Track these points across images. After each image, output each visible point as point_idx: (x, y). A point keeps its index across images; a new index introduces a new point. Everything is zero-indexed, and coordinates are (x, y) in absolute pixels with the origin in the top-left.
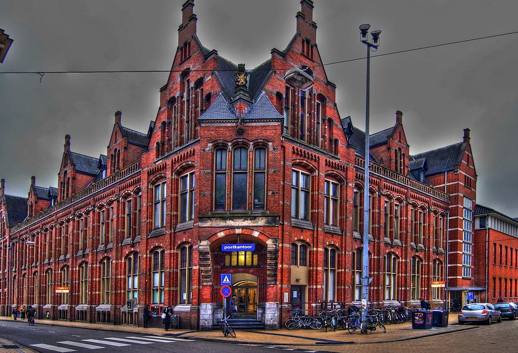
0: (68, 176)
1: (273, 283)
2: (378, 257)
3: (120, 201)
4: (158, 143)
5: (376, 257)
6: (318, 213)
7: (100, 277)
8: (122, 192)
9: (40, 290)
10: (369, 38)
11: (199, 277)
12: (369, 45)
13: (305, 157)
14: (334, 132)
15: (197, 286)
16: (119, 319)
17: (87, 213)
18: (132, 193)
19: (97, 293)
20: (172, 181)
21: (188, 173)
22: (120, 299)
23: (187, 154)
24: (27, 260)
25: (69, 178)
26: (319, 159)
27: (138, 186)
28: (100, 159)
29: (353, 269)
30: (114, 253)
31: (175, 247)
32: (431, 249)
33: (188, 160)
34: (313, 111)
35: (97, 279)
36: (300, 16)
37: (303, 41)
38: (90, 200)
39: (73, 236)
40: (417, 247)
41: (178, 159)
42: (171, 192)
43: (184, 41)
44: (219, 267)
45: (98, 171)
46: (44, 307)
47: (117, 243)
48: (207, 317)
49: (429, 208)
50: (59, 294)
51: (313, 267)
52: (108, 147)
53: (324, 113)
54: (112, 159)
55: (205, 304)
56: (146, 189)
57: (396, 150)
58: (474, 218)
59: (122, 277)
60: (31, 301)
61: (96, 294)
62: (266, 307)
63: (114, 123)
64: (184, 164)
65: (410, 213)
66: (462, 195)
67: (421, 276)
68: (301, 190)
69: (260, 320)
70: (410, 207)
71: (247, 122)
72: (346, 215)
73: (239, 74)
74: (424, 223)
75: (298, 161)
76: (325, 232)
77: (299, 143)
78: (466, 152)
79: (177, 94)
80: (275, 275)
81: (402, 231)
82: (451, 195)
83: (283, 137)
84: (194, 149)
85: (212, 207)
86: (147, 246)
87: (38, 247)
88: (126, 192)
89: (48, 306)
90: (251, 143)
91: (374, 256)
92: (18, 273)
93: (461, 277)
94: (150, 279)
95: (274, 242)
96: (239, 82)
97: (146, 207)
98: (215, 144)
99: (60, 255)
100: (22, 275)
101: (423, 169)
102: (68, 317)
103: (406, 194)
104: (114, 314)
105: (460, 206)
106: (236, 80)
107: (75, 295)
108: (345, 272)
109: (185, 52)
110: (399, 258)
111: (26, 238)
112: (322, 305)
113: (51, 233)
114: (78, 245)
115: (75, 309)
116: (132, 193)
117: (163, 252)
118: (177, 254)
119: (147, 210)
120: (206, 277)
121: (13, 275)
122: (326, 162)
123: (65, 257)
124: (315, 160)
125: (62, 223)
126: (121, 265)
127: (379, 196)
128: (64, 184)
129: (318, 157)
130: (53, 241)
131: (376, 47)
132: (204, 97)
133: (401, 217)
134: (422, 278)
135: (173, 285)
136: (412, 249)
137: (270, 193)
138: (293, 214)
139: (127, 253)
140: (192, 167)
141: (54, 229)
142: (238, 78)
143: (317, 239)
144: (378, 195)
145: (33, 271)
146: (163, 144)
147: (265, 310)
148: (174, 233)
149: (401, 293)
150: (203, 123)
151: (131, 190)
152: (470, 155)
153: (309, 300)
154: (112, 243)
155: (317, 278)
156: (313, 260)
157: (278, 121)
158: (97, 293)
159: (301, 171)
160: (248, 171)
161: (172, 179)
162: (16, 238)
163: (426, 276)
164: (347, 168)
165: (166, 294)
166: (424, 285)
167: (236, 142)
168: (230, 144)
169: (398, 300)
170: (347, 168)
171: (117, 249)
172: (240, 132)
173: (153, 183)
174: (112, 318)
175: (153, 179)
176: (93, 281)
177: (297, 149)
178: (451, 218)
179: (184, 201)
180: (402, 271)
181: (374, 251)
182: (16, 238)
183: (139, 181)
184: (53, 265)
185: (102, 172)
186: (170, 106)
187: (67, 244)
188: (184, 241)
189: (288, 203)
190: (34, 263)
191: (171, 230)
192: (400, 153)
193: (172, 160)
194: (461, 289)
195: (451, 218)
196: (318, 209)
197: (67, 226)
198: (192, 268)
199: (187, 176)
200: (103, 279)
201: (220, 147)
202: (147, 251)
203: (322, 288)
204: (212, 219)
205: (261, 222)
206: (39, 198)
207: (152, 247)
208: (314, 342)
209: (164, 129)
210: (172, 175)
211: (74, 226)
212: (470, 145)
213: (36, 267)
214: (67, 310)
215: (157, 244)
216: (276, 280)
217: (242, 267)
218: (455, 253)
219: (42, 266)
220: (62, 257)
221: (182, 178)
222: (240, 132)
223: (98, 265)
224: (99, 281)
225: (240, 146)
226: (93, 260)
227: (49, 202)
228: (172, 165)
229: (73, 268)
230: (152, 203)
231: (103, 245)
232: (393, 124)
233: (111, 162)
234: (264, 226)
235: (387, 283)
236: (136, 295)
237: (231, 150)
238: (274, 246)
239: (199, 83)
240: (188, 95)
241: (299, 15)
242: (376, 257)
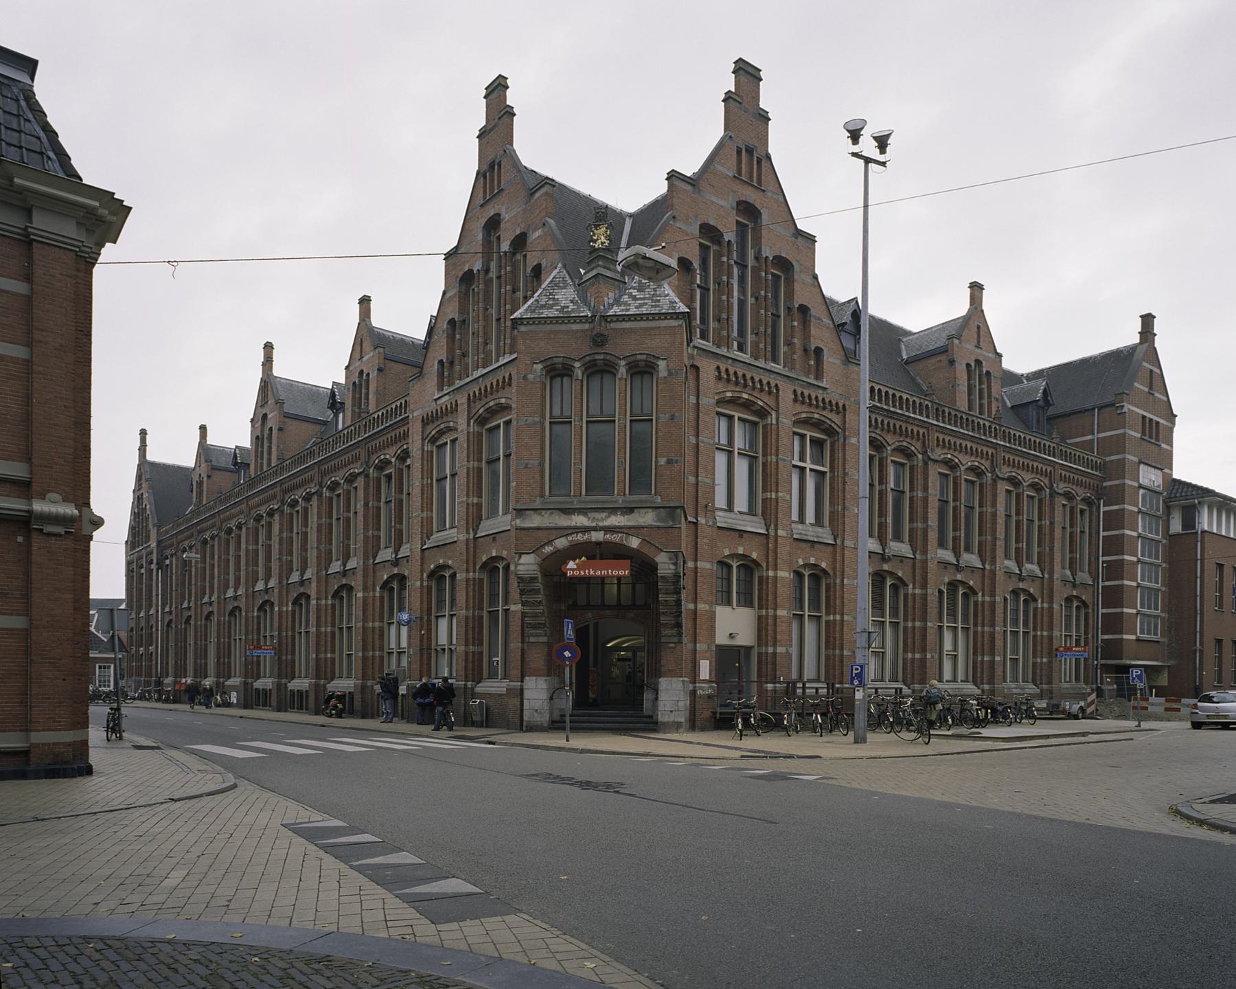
0: (269, 425)
1: (675, 639)
2: (924, 592)
3: (371, 476)
4: (441, 362)
5: (918, 591)
6: (777, 499)
7: (333, 625)
8: (478, 405)
9: (218, 649)
10: (868, 146)
11: (522, 627)
12: (868, 160)
13: (745, 386)
14: (812, 332)
15: (520, 644)
16: (372, 708)
17: (308, 498)
18: (393, 460)
19: (329, 655)
20: (468, 436)
21: (501, 421)
22: (373, 668)
23: (498, 385)
24: (193, 591)
25: (271, 429)
26: (778, 390)
27: (405, 447)
28: (332, 390)
29: (941, 620)
30: (360, 577)
31: (477, 568)
32: (1056, 576)
33: (500, 395)
34: (763, 293)
35: (329, 629)
36: (731, 100)
37: (739, 152)
38: (312, 472)
39: (280, 544)
40: (1020, 570)
41: (480, 393)
42: (468, 457)
43: (490, 158)
44: (563, 608)
45: (330, 415)
46: (226, 683)
47: (366, 558)
48: (537, 705)
49: (1051, 487)
50: (255, 659)
51: (767, 609)
52: (347, 368)
53: (790, 295)
54: (354, 391)
55: (534, 678)
56: (420, 452)
57: (968, 365)
58: (1168, 509)
59: (377, 624)
60: (201, 672)
61: (326, 659)
62: (660, 688)
63: (358, 321)
64: (492, 404)
65: (1001, 498)
66: (1135, 459)
67: (1032, 633)
68: (739, 453)
69: (650, 713)
70: (1003, 487)
71: (612, 321)
72: (844, 503)
73: (597, 227)
74: (1040, 519)
75: (804, 415)
76: (795, 539)
77: (732, 359)
78: (1145, 364)
79: (477, 266)
80: (679, 625)
81: (984, 538)
82: (1108, 459)
83: (695, 347)
84: (510, 374)
85: (542, 487)
86: (422, 565)
87: (213, 565)
88: (382, 457)
89: (235, 681)
90: (623, 363)
91: (914, 588)
92: (176, 616)
93: (1133, 637)
94: (429, 630)
95: (670, 559)
96: (595, 241)
97: (420, 488)
98: (547, 366)
99: (228, 587)
100: (184, 620)
101: (1041, 403)
102: (274, 703)
103: (992, 459)
104: (362, 698)
105: (1128, 482)
106: (589, 238)
107: (286, 660)
108: (842, 620)
109: (492, 180)
110: (975, 593)
111: (191, 548)
112: (788, 686)
113: (239, 537)
114: (292, 561)
115: (286, 687)
116: (393, 460)
117: (453, 576)
118: (481, 580)
119: (422, 494)
120: (535, 627)
121: (167, 620)
122: (796, 395)
123: (267, 585)
124: (770, 393)
125: (258, 518)
126: (374, 600)
127: (926, 464)
128: (263, 439)
129: (776, 386)
130: (243, 553)
131: (883, 164)
132: (529, 270)
133: (980, 506)
134: (1035, 636)
135: (473, 642)
136: (1009, 574)
137: (662, 461)
138: (720, 500)
139: (385, 577)
140: (506, 408)
141: (244, 530)
142: (594, 235)
143: (776, 554)
144: (923, 460)
145: (205, 612)
146: (452, 363)
147: (657, 694)
148: (475, 539)
149: (982, 668)
150: (522, 324)
151: (390, 454)
152: (1157, 371)
153: (759, 675)
154: (356, 558)
155: (775, 632)
156: (767, 595)
157: (678, 318)
158: (329, 655)
159: (737, 415)
160: (617, 419)
161: (468, 433)
162: (172, 545)
163: (1045, 633)
164: (844, 406)
165: (460, 660)
166: (1042, 652)
167: (590, 361)
168: (577, 365)
169: (975, 683)
170: (844, 406)
171: (365, 570)
172: (599, 340)
173: (433, 440)
174: (357, 704)
175: (433, 432)
176: (321, 633)
177: (727, 370)
178: (1107, 508)
179: (495, 475)
180: (983, 620)
181: (914, 576)
182: (172, 545)
183: (406, 435)
184: (244, 600)
185: (336, 416)
186: (464, 288)
187: (304, 548)
188: (494, 554)
189: (707, 480)
190: (207, 596)
191: (468, 533)
192: (981, 371)
193: (469, 395)
194: (1128, 662)
195: (1107, 508)
196: (777, 492)
197: (270, 525)
198: (509, 609)
199: (499, 426)
200: (341, 629)
201: (557, 371)
202: (422, 575)
203: (787, 652)
204: (543, 513)
205: (647, 518)
206: (214, 468)
207: (432, 566)
208: (738, 754)
209: (454, 335)
210: (469, 425)
211: (281, 525)
212: (1155, 349)
213: (211, 603)
214: (270, 690)
215: (441, 561)
216: (680, 634)
217: (610, 607)
218: (1118, 585)
219: (222, 602)
220: (295, 577)
221: (490, 430)
222: (599, 340)
223: (330, 602)
224: (333, 634)
225: (600, 369)
226: (318, 592)
227: (235, 476)
228: (469, 405)
229: (280, 605)
230: (432, 479)
231: (339, 563)
232: (961, 308)
233: (354, 397)
234: (651, 527)
235: (948, 646)
236: (404, 663)
237: (580, 378)
238: (672, 567)
239: (520, 242)
240: (500, 267)
241: (730, 97)
242: (918, 591)
